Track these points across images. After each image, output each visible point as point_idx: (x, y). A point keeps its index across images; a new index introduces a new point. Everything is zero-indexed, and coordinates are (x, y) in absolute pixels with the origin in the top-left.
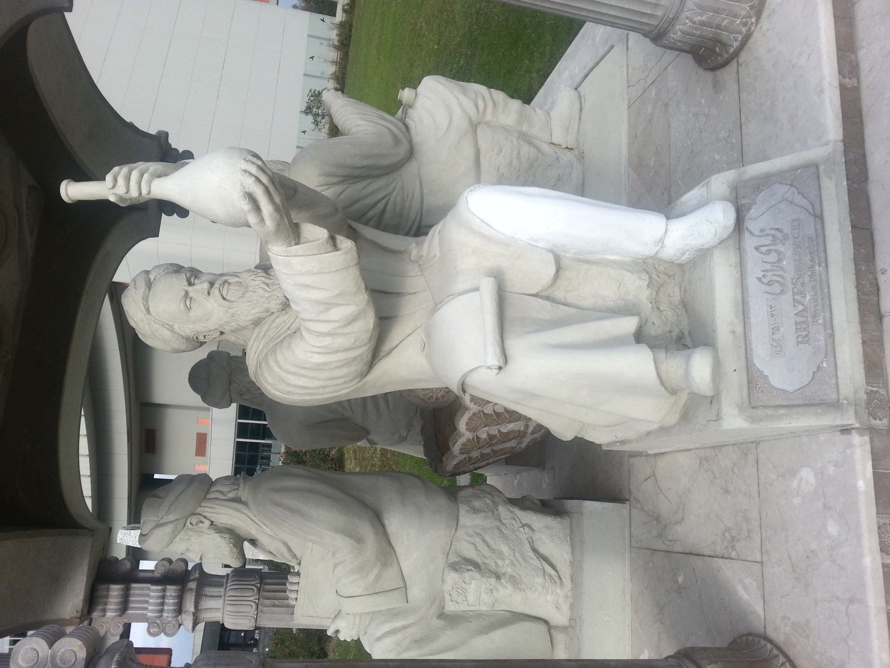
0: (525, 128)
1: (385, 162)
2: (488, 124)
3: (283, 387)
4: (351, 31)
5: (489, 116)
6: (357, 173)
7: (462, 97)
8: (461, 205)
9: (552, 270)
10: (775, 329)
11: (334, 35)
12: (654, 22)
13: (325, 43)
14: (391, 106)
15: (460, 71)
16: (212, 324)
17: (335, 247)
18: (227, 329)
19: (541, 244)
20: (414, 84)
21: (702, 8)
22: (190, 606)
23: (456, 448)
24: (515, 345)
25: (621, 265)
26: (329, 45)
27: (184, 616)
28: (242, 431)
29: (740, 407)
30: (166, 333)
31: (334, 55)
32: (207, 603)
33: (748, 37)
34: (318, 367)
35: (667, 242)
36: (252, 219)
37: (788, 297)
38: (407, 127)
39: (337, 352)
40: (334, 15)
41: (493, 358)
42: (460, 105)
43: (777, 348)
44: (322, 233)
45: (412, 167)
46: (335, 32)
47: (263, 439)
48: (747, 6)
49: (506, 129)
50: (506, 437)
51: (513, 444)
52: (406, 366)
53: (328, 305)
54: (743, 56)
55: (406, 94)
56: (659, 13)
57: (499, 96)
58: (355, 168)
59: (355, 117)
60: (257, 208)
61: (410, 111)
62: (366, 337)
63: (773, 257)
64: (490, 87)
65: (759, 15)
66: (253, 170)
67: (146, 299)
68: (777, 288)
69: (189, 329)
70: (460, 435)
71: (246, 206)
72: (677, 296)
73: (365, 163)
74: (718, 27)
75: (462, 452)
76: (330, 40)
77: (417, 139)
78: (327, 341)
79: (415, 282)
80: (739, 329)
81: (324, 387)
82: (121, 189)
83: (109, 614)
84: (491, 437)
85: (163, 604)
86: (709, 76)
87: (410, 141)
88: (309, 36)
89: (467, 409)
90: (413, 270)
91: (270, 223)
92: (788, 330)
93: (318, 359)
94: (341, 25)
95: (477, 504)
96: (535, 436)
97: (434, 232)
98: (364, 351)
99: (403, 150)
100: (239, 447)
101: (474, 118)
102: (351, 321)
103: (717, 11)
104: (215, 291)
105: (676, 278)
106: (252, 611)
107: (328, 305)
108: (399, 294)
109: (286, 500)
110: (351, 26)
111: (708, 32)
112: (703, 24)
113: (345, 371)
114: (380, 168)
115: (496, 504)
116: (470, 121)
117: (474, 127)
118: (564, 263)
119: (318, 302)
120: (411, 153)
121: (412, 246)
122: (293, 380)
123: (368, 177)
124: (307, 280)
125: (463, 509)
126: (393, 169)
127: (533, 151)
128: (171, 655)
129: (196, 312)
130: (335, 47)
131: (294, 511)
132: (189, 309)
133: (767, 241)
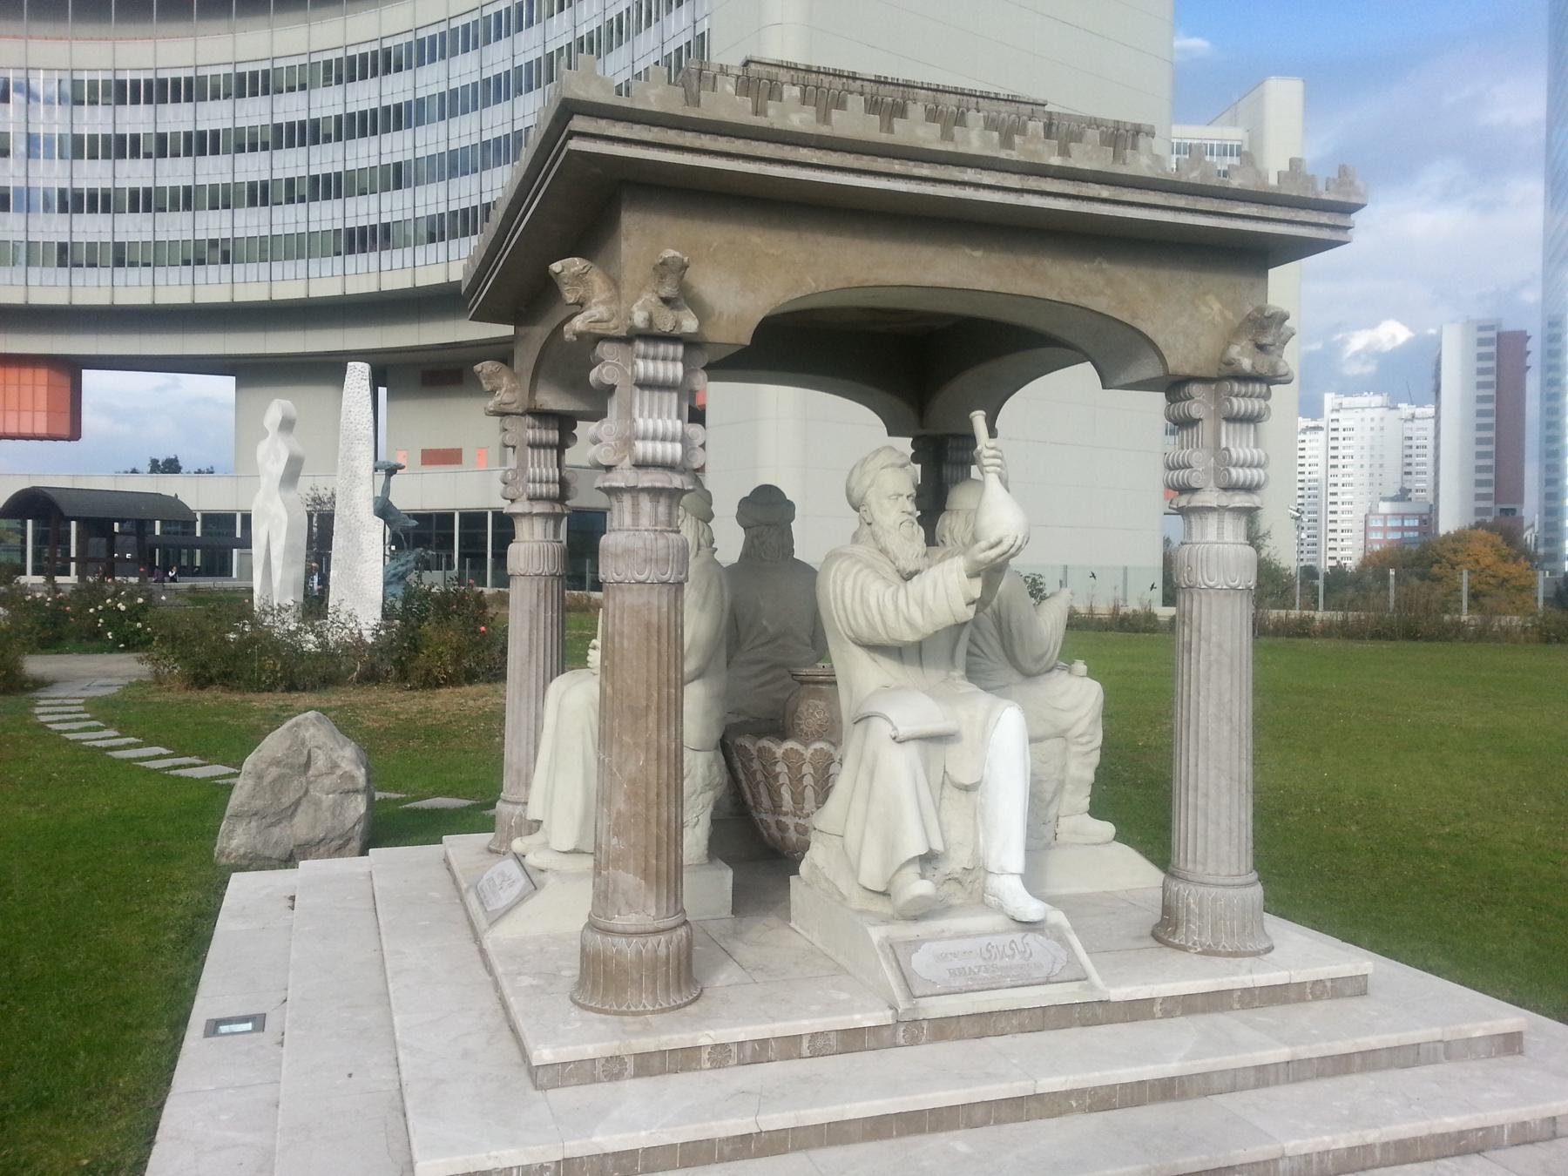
0: (1069, 787)
1: (1018, 650)
2: (1066, 749)
3: (840, 576)
4: (1145, 631)
5: (1075, 749)
6: (1004, 625)
7: (1087, 721)
8: (1006, 702)
9: (967, 782)
10: (955, 955)
11: (1133, 606)
12: (1181, 865)
13: (1120, 593)
14: (1067, 657)
15: (1109, 715)
16: (878, 515)
17: (968, 604)
18: (875, 528)
19: (986, 771)
20: (1091, 674)
21: (1200, 903)
22: (538, 508)
23: (765, 743)
24: (912, 749)
25: (976, 844)
26: (1116, 600)
27: (527, 503)
28: (473, 520)
29: (887, 938)
30: (867, 482)
31: (1103, 609)
32: (538, 525)
33: (1183, 949)
34: (863, 601)
35: (1003, 878)
36: (983, 544)
37: (981, 963)
38: (1050, 670)
39: (882, 615)
40: (1165, 604)
41: (903, 731)
42: (1080, 719)
43: (942, 957)
44: (977, 593)
45: (1017, 677)
46: (1138, 608)
47: (493, 555)
48: (1209, 942)
49: (1064, 768)
50: (774, 793)
51: (765, 801)
52: (861, 677)
53: (922, 604)
54: (1168, 950)
55: (1081, 667)
56: (1190, 866)
57: (1095, 758)
58: (1009, 623)
59: (1049, 622)
60: (992, 547)
61: (1065, 673)
62: (897, 636)
63: (1009, 952)
64: (1102, 748)
65: (1204, 953)
66: (1019, 542)
67: (893, 465)
68: (987, 955)
69: (871, 498)
70: (779, 746)
71: (993, 540)
72: (955, 901)
73: (1015, 631)
74: (1188, 921)
75: (760, 750)
76: (1125, 600)
77: (1041, 679)
78: (890, 607)
79: (934, 675)
80: (946, 934)
81: (845, 609)
82: (986, 453)
83: (530, 433)
84: (776, 777)
85: (541, 482)
86: (1147, 931)
87: (1039, 674)
88: (1126, 569)
89: (806, 746)
90: (942, 674)
91: (981, 556)
92: (956, 964)
93: (873, 602)
94: (1151, 617)
95: (715, 768)
96: (773, 826)
97: (972, 688)
98: (883, 638)
99: (1030, 666)
100: (445, 518)
101: (1069, 734)
102: (910, 623)
103: (1201, 916)
104: (906, 517)
105: (972, 885)
106: (533, 570)
107: (922, 604)
108: (921, 665)
109: (714, 591)
110: (1153, 631)
111: (1182, 914)
112: (1188, 906)
113: (877, 618)
114: (1011, 645)
115: (713, 788)
116: (1067, 730)
117: (1062, 735)
118: (972, 795)
119: (923, 596)
120: (1028, 675)
121: (959, 673)
122: (849, 584)
123: (1002, 639)
124: (940, 586)
125: (710, 755)
126: (1013, 660)
127: (1048, 796)
128: (69, 440)
129: (887, 504)
130: (1116, 608)
131: (705, 597)
132: (889, 497)
133: (1021, 948)
